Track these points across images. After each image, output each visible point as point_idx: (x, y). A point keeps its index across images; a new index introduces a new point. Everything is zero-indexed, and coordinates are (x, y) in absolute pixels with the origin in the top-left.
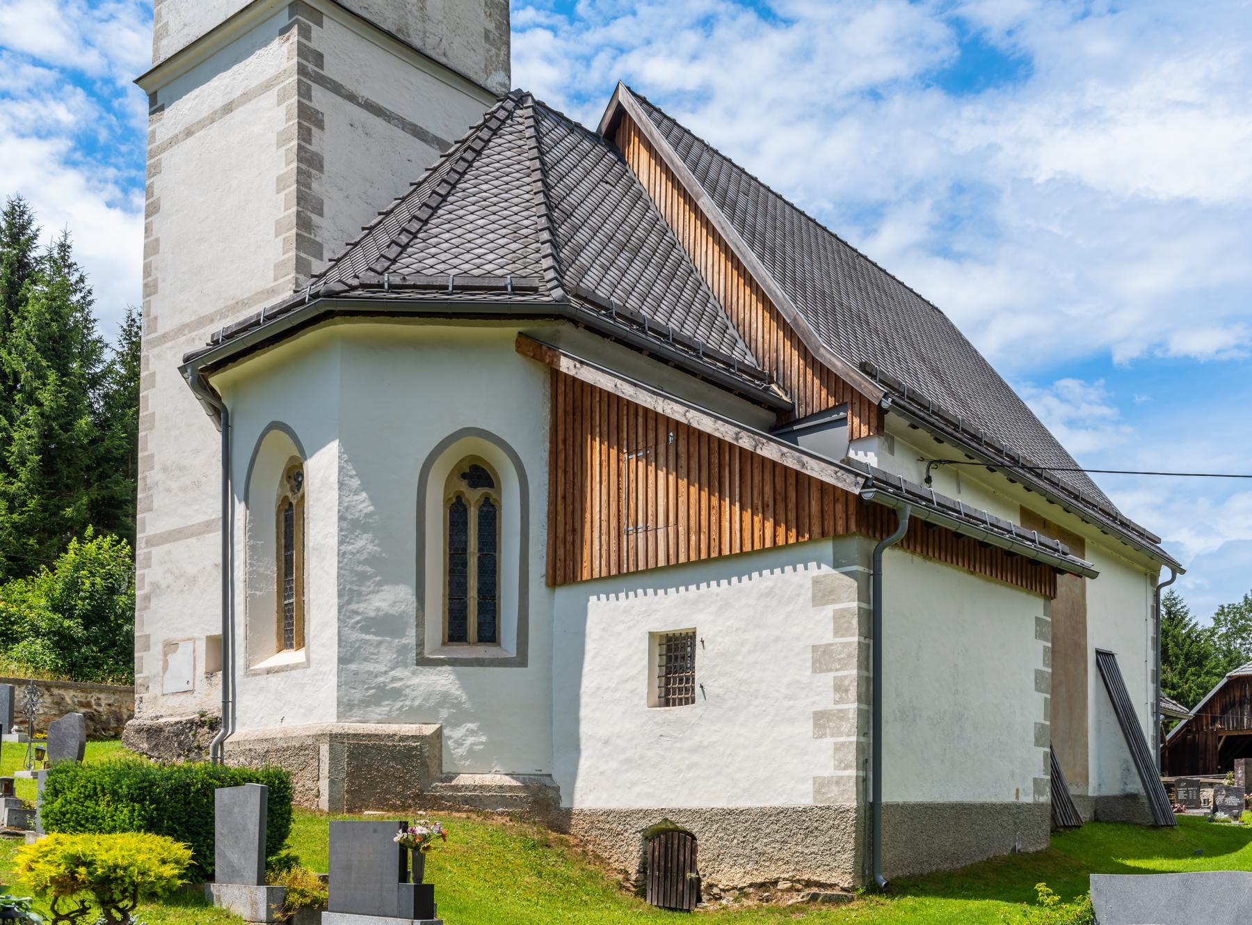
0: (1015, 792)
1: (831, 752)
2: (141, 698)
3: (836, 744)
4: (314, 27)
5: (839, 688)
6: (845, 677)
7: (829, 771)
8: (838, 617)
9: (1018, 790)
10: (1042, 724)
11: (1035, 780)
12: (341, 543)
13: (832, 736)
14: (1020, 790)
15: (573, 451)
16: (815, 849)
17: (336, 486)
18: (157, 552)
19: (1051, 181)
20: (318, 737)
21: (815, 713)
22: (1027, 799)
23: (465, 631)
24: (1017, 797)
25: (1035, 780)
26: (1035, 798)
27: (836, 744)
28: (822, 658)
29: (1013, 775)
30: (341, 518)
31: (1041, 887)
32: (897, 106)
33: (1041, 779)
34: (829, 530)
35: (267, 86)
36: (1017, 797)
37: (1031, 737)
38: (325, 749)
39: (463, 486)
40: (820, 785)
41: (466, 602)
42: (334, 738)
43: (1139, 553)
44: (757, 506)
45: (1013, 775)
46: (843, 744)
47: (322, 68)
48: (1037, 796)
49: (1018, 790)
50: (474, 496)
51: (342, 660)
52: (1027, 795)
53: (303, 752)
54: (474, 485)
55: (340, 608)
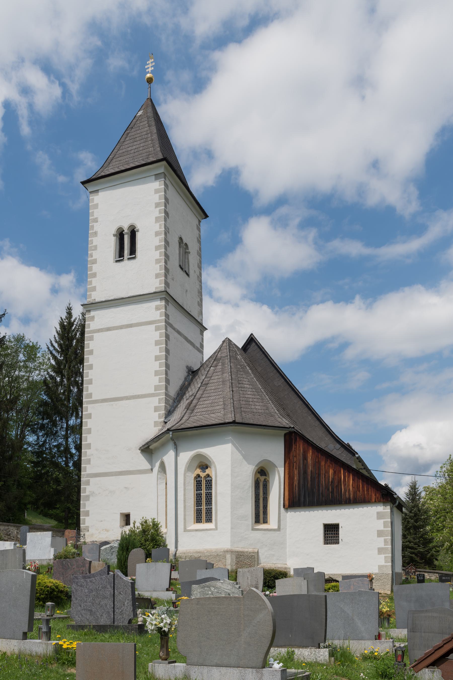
1: (384, 558)
2: (85, 534)
3: (385, 556)
5: (385, 541)
6: (388, 539)
7: (383, 563)
8: (385, 523)
12: (232, 492)
13: (383, 554)
15: (175, 425)
16: (379, 584)
17: (230, 475)
18: (92, 480)
19: (353, 298)
20: (227, 551)
21: (378, 548)
23: (259, 520)
27: (385, 556)
28: (380, 534)
30: (232, 485)
39: (259, 475)
40: (380, 567)
41: (259, 511)
42: (232, 552)
46: (387, 556)
50: (262, 478)
51: (232, 528)
53: (218, 557)
54: (261, 475)
55: (231, 512)
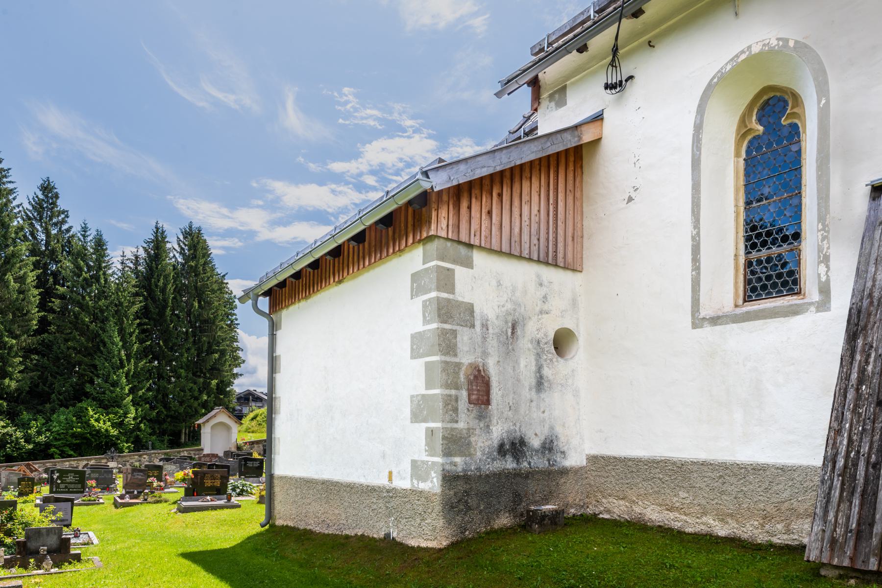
0: (387, 474)
4: (460, 272)
9: (390, 473)
10: (423, 396)
11: (414, 463)
14: (394, 474)
22: (403, 483)
24: (390, 479)
25: (414, 463)
26: (412, 484)
29: (384, 456)
31: (228, 389)
32: (468, 147)
33: (423, 462)
34: (841, 451)
35: (577, 326)
36: (390, 479)
37: (407, 412)
38: (183, 440)
43: (279, 264)
44: (836, 485)
45: (384, 456)
47: (452, 291)
48: (415, 482)
49: (390, 473)
52: (403, 479)
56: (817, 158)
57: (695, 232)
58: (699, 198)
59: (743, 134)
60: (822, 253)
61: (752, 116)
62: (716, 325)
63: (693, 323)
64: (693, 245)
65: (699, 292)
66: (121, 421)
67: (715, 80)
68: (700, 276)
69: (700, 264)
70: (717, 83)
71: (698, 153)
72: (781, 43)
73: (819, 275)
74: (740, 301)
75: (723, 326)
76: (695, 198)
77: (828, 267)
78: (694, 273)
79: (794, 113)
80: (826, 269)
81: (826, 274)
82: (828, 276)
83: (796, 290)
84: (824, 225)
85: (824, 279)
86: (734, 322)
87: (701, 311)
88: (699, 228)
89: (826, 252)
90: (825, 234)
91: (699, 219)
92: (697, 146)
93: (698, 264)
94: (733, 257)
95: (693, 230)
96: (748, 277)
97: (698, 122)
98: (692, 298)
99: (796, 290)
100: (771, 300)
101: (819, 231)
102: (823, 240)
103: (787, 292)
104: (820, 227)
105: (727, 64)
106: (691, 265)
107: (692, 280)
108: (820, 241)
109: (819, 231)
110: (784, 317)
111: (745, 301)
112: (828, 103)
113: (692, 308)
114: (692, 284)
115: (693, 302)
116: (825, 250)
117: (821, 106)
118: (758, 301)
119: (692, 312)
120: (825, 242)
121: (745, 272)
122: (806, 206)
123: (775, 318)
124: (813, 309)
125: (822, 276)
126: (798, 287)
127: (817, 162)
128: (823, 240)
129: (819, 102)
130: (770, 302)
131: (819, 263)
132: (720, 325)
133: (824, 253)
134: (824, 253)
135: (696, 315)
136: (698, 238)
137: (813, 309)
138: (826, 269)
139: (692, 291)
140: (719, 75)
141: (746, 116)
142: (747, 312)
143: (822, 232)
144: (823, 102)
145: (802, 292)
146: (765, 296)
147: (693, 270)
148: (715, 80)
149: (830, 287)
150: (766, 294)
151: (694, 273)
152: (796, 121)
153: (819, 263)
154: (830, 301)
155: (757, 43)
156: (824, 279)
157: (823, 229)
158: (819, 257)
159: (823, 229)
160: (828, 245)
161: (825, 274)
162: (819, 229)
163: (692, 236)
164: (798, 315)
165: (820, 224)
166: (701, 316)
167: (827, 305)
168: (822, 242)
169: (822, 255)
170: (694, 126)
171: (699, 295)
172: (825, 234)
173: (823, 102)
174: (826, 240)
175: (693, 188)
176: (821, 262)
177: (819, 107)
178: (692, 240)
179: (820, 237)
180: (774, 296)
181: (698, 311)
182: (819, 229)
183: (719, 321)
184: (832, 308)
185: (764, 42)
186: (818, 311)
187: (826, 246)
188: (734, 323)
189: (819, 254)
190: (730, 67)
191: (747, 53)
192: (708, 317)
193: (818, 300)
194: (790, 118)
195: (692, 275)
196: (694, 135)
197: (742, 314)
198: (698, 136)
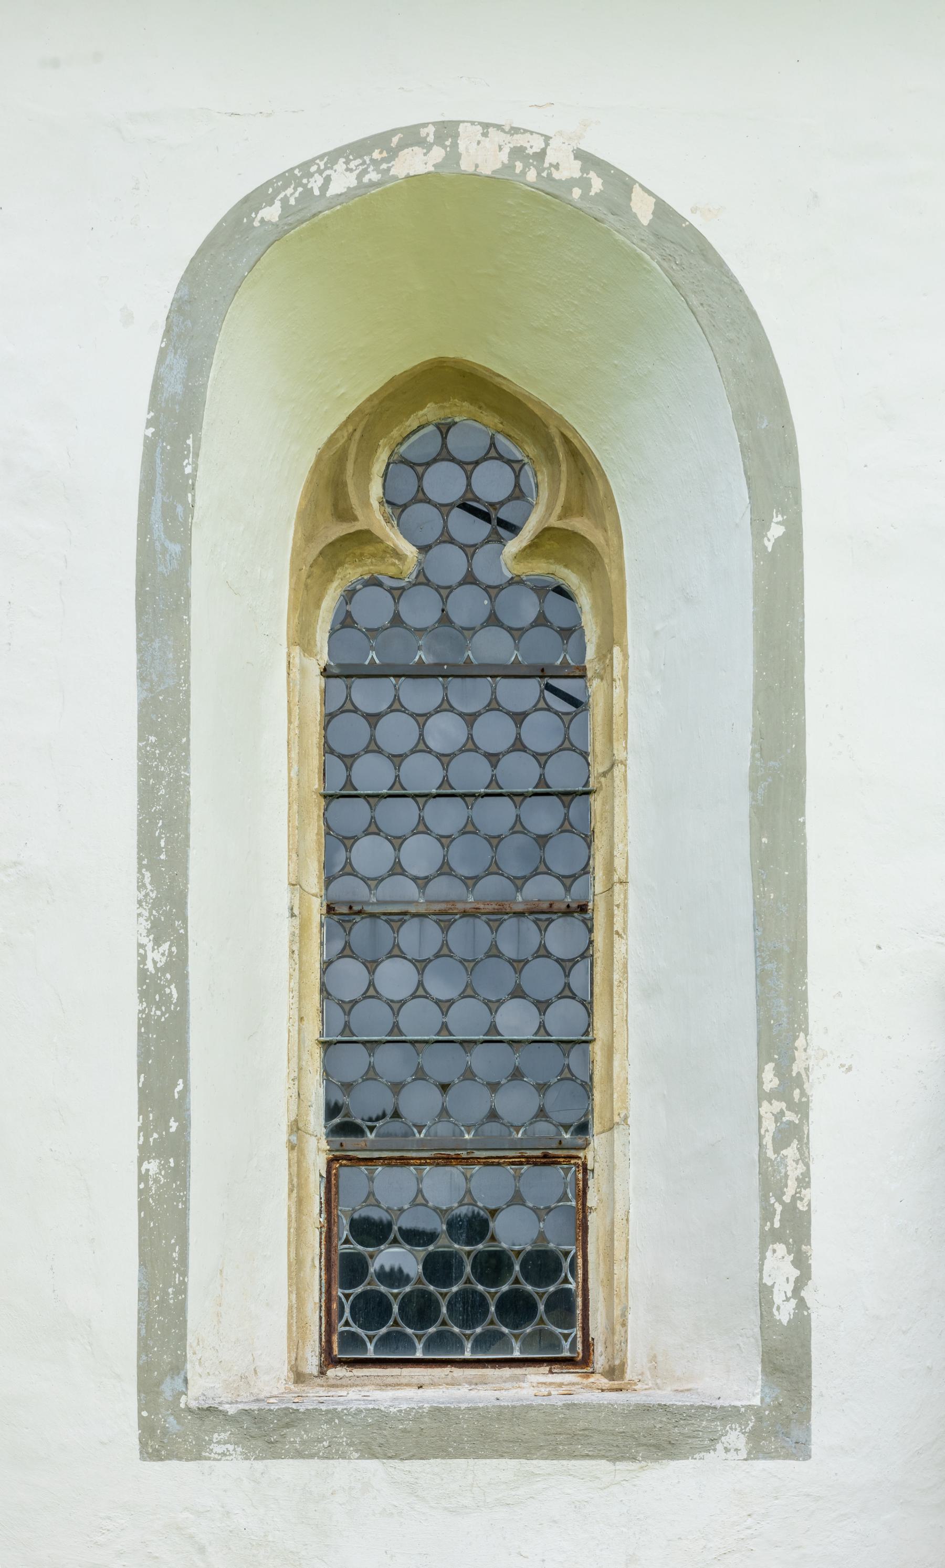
56: (753, 768)
57: (157, 956)
58: (180, 786)
59: (332, 544)
60: (779, 1200)
61: (368, 479)
62: (276, 1456)
63: (148, 1429)
64: (145, 1022)
65: (184, 1274)
66: (365, 168)
67: (272, 213)
68: (185, 1186)
69: (184, 1128)
70: (279, 233)
71: (175, 548)
72: (597, 184)
73: (765, 1293)
74: (312, 1361)
75: (315, 1463)
76: (159, 776)
77: (801, 1262)
78: (152, 1166)
79: (571, 538)
80: (797, 1273)
81: (797, 1291)
82: (802, 1304)
83: (566, 1345)
84: (783, 1072)
85: (784, 1313)
86: (369, 1452)
87: (192, 1369)
88: (182, 942)
89: (794, 1198)
90: (790, 1116)
91: (183, 895)
92: (168, 512)
93: (174, 1126)
94: (283, 1135)
95: (148, 942)
96: (343, 1248)
97: (174, 387)
98: (145, 1294)
99: (566, 1345)
100: (458, 1372)
101: (763, 1096)
102: (781, 1141)
103: (427, 1348)
104: (770, 1081)
105: (332, 157)
106: (134, 1121)
107: (143, 1205)
108: (768, 1140)
109: (763, 1096)
110: (614, 1459)
111: (329, 1360)
112: (794, 535)
113: (143, 1346)
114: (142, 1224)
115: (146, 1320)
116: (792, 1186)
117: (769, 546)
118: (395, 1371)
119: (144, 1370)
120: (791, 1152)
121: (329, 1220)
122: (625, 972)
123: (572, 1456)
124: (735, 1438)
125: (778, 1298)
126: (578, 1332)
127: (753, 788)
128: (781, 1141)
129: (760, 526)
130: (473, 1383)
131: (768, 1238)
132: (299, 1455)
133: (787, 1199)
134: (787, 1199)
135: (168, 1387)
136: (174, 991)
137: (735, 1438)
138: (797, 1273)
139: (143, 1263)
140: (292, 194)
141: (350, 467)
142: (438, 1412)
143: (779, 1105)
144: (776, 531)
145: (600, 1359)
146: (427, 1348)
147: (145, 1153)
148: (272, 213)
149: (808, 1354)
150: (432, 1343)
151: (152, 1166)
152: (571, 579)
153: (768, 1238)
154: (805, 1417)
155: (486, 126)
156: (784, 1313)
157: (782, 1094)
158: (767, 1214)
159: (782, 1094)
160: (801, 1168)
161: (789, 1288)
162: (767, 1087)
163: (143, 975)
164: (672, 1456)
165: (769, 1067)
166: (191, 1399)
167: (796, 1433)
168: (776, 1151)
169: (779, 1208)
170: (154, 403)
171: (182, 1289)
172: (790, 1116)
173: (776, 531)
174: (795, 1143)
175: (146, 726)
176: (775, 1236)
177: (758, 548)
178: (144, 995)
179: (769, 1125)
180: (468, 1355)
181: (178, 1368)
182: (767, 1087)
183: (295, 1437)
184: (814, 1449)
185: (520, 140)
186: (757, 1451)
187: (794, 1171)
188: (374, 1456)
189: (764, 1198)
190: (351, 180)
191: (438, 154)
192: (231, 1410)
193: (756, 1401)
194: (548, 556)
195: (143, 1177)
196: (150, 447)
197: (416, 1416)
198: (175, 459)
